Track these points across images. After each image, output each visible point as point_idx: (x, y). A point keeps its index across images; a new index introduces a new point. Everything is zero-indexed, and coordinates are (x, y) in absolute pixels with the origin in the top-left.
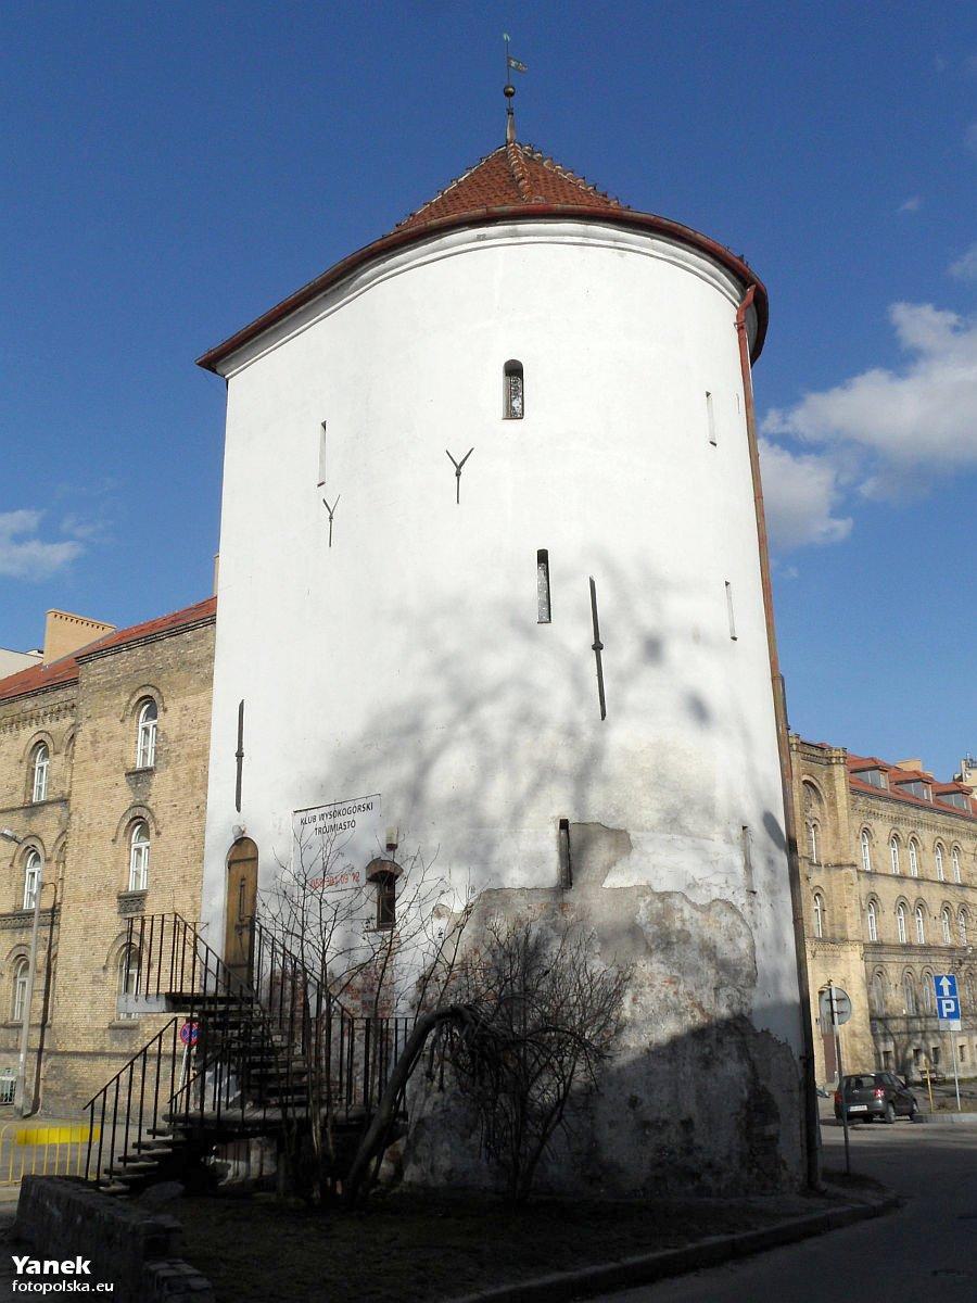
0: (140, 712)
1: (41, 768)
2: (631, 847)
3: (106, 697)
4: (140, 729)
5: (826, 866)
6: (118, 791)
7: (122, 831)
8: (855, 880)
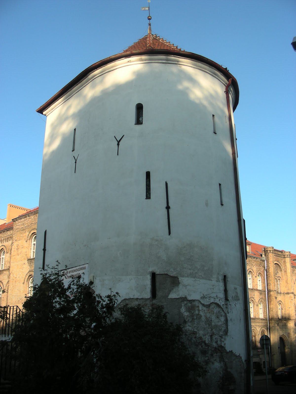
0: (32, 239)
1: (3, 258)
2: (179, 283)
3: (21, 233)
4: (32, 244)
5: (283, 293)
6: (25, 266)
8: (293, 298)
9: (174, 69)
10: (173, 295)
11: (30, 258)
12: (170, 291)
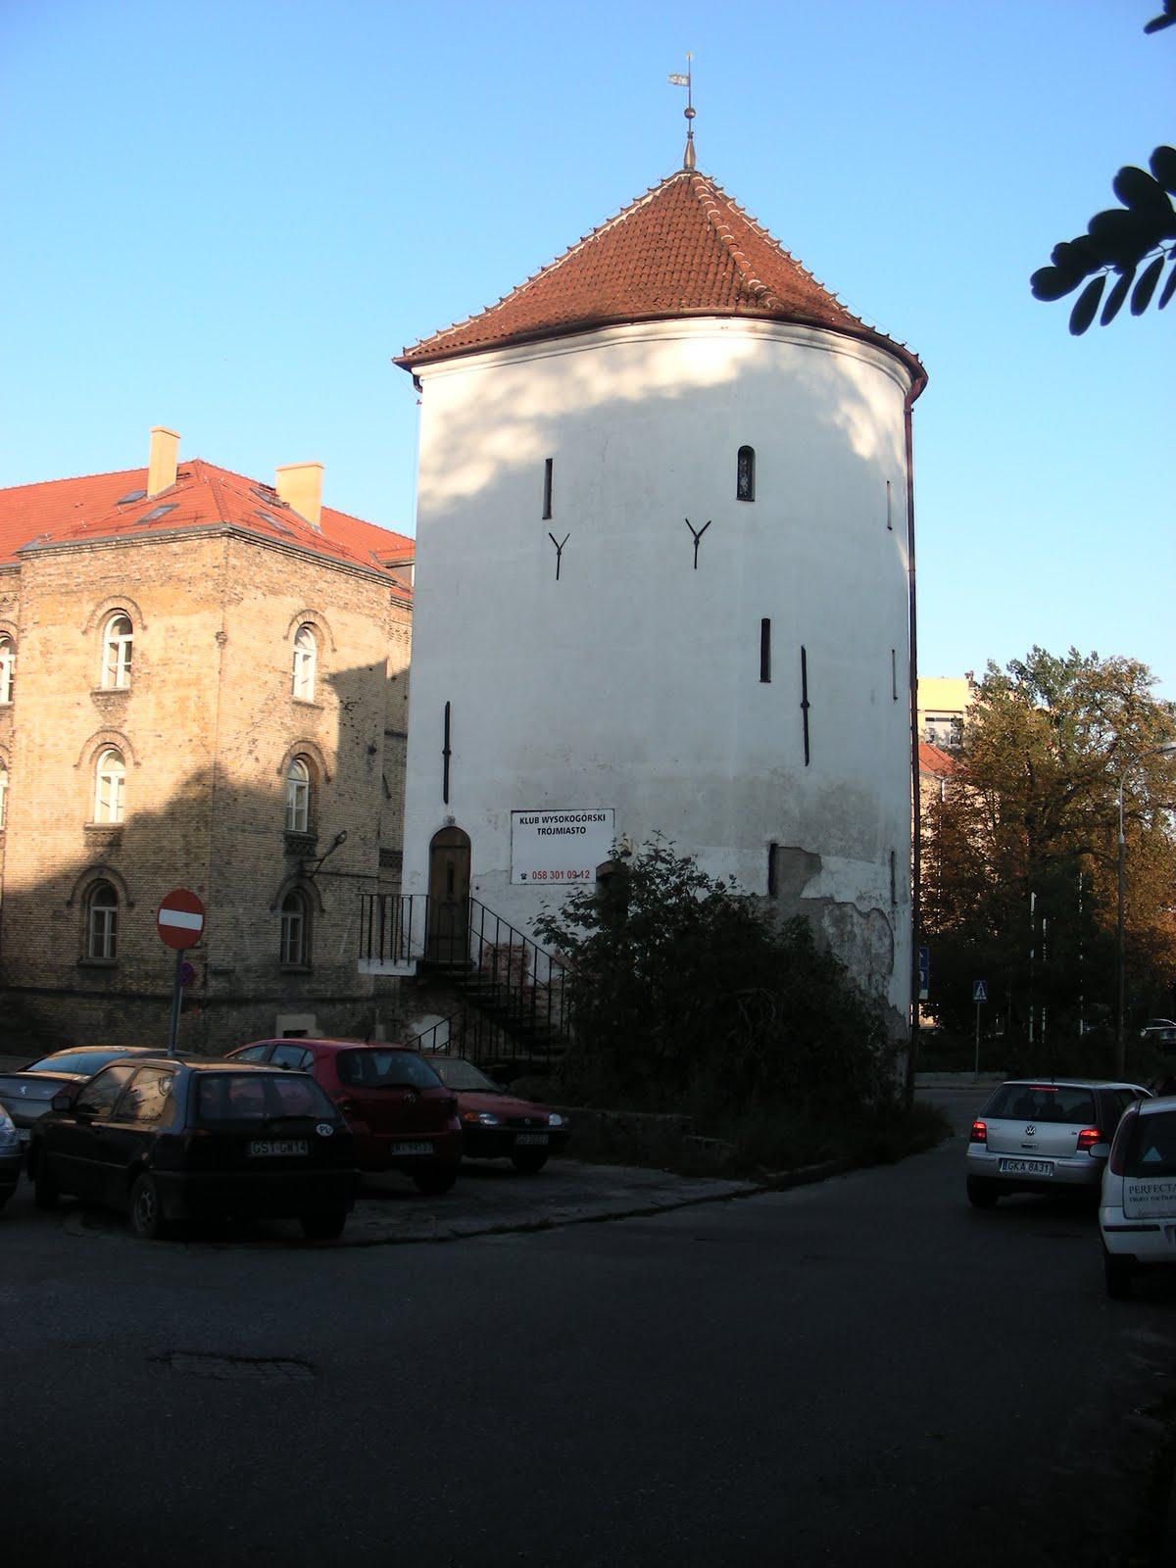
6: (80, 712)
7: (87, 757)
9: (818, 362)
10: (809, 893)
11: (100, 688)
12: (805, 883)
